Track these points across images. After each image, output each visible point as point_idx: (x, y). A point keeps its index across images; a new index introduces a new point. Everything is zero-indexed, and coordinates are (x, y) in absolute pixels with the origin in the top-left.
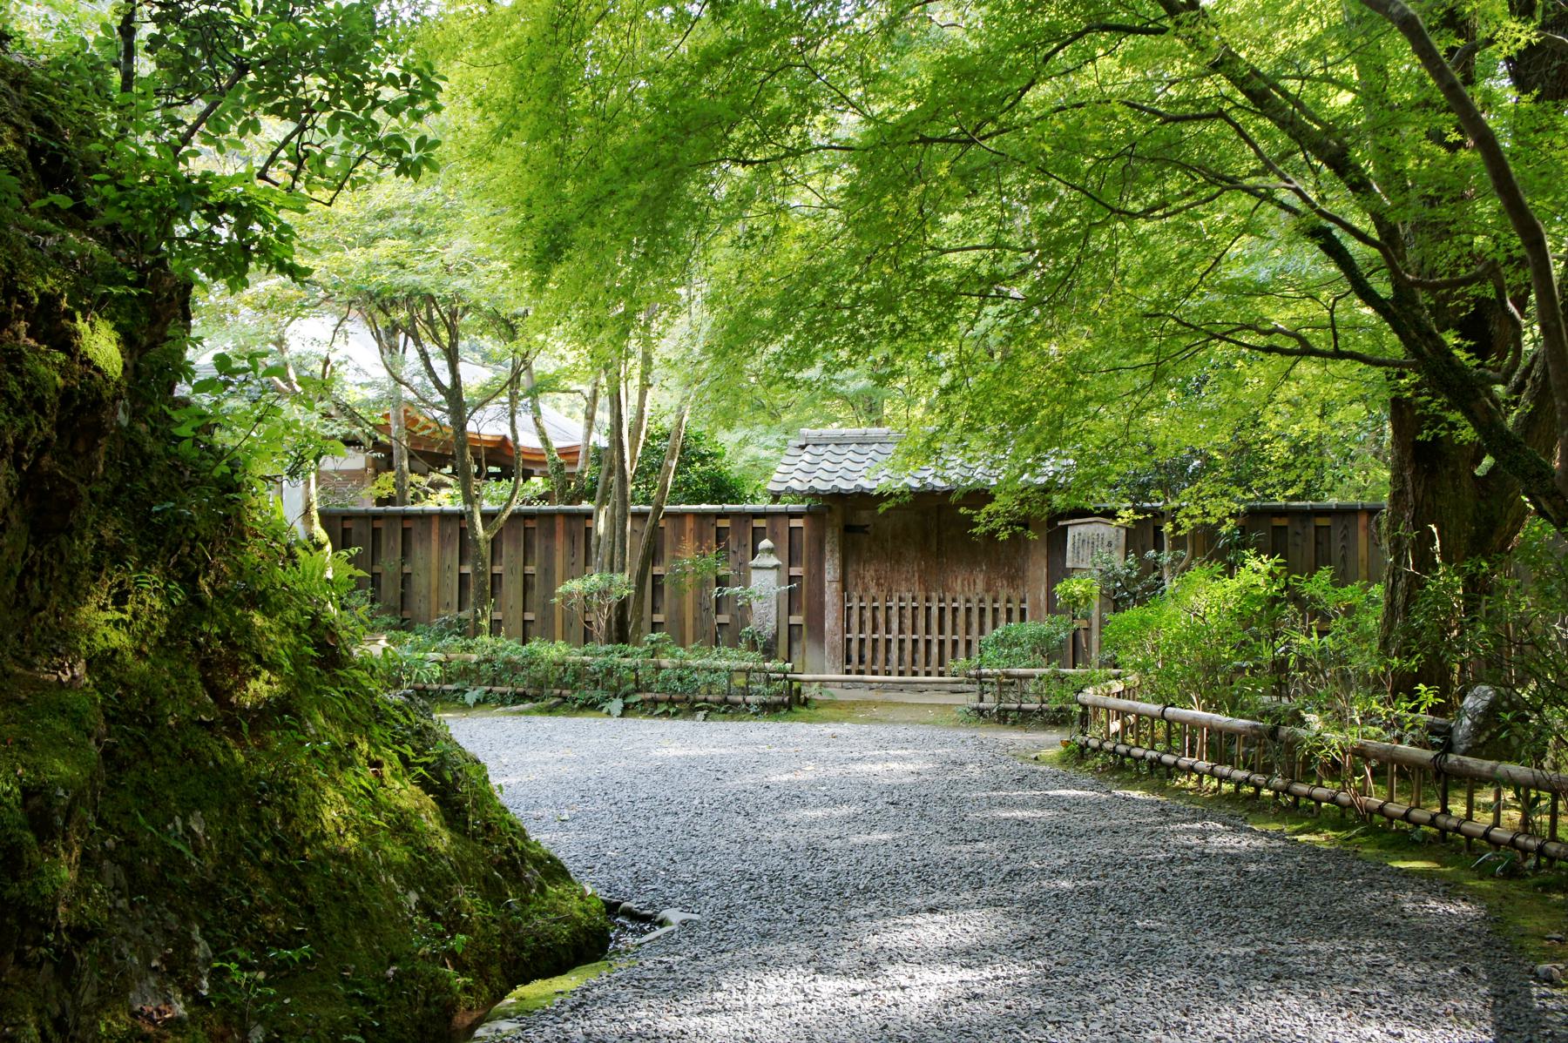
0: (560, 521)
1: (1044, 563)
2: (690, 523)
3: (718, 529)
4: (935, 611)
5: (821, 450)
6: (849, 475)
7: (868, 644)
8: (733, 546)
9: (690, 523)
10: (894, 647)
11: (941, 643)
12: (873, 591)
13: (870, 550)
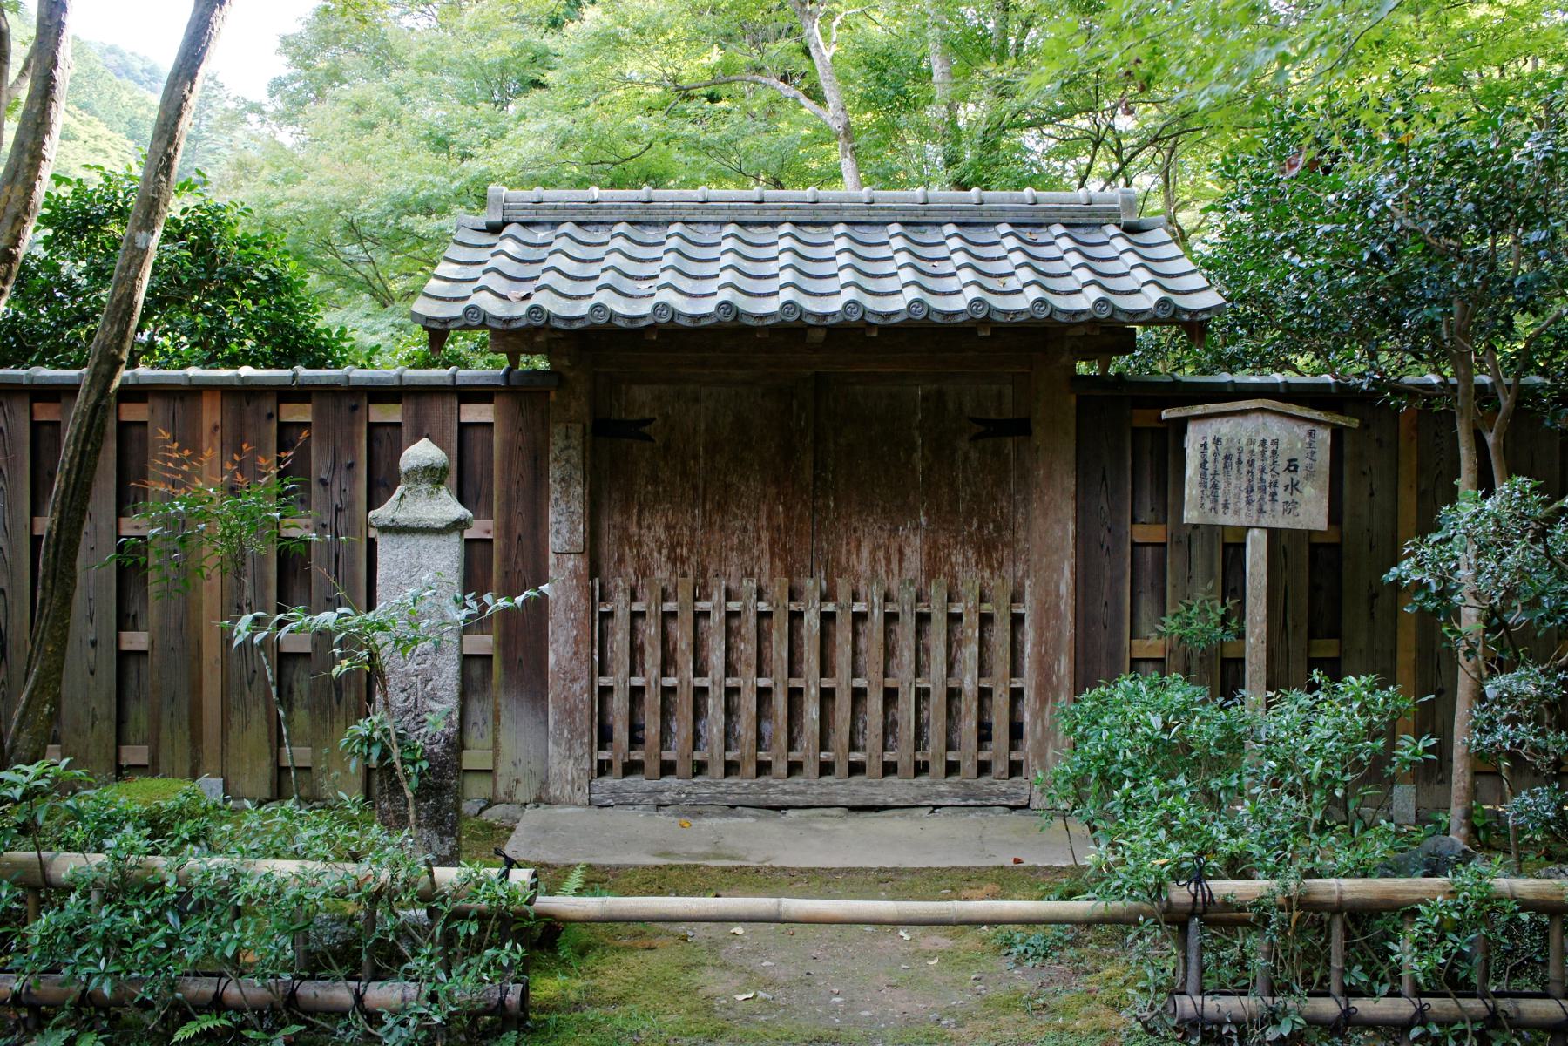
1: (1068, 509)
2: (211, 413)
3: (283, 427)
4: (812, 621)
5: (541, 235)
6: (628, 286)
7: (652, 700)
8: (319, 465)
9: (211, 413)
10: (715, 704)
11: (827, 695)
12: (662, 574)
13: (654, 479)
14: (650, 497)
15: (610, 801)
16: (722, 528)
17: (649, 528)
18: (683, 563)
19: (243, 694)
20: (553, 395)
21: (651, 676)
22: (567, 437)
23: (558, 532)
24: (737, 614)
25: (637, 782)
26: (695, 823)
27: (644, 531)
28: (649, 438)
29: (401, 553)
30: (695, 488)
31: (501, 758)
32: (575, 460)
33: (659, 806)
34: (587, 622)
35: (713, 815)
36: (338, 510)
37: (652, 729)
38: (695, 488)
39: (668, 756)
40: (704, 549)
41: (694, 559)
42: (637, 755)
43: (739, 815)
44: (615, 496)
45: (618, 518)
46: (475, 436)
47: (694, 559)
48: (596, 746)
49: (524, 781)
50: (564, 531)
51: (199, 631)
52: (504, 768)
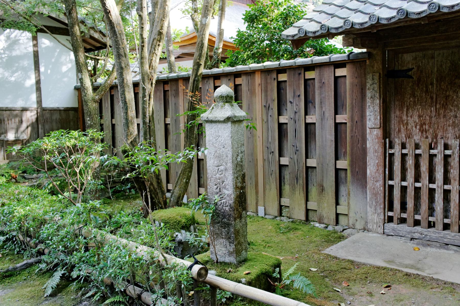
0: (258, 79)
7: (411, 193)
13: (413, 95)
14: (412, 103)
15: (392, 234)
16: (444, 116)
17: (411, 117)
18: (426, 132)
19: (269, 178)
20: (367, 61)
21: (410, 181)
22: (373, 79)
23: (370, 119)
24: (449, 156)
25: (404, 228)
26: (422, 248)
27: (409, 118)
28: (411, 77)
29: (213, 130)
30: (432, 98)
31: (351, 210)
32: (376, 89)
33: (412, 239)
34: (382, 158)
35: (436, 246)
36: (296, 112)
37: (410, 204)
38: (432, 98)
39: (417, 217)
40: (436, 126)
41: (431, 131)
42: (404, 215)
43: (447, 249)
44: (397, 103)
45: (398, 113)
46: (340, 81)
47: (431, 131)
48: (386, 210)
49: (359, 220)
50: (372, 119)
51: (257, 156)
52: (351, 215)
